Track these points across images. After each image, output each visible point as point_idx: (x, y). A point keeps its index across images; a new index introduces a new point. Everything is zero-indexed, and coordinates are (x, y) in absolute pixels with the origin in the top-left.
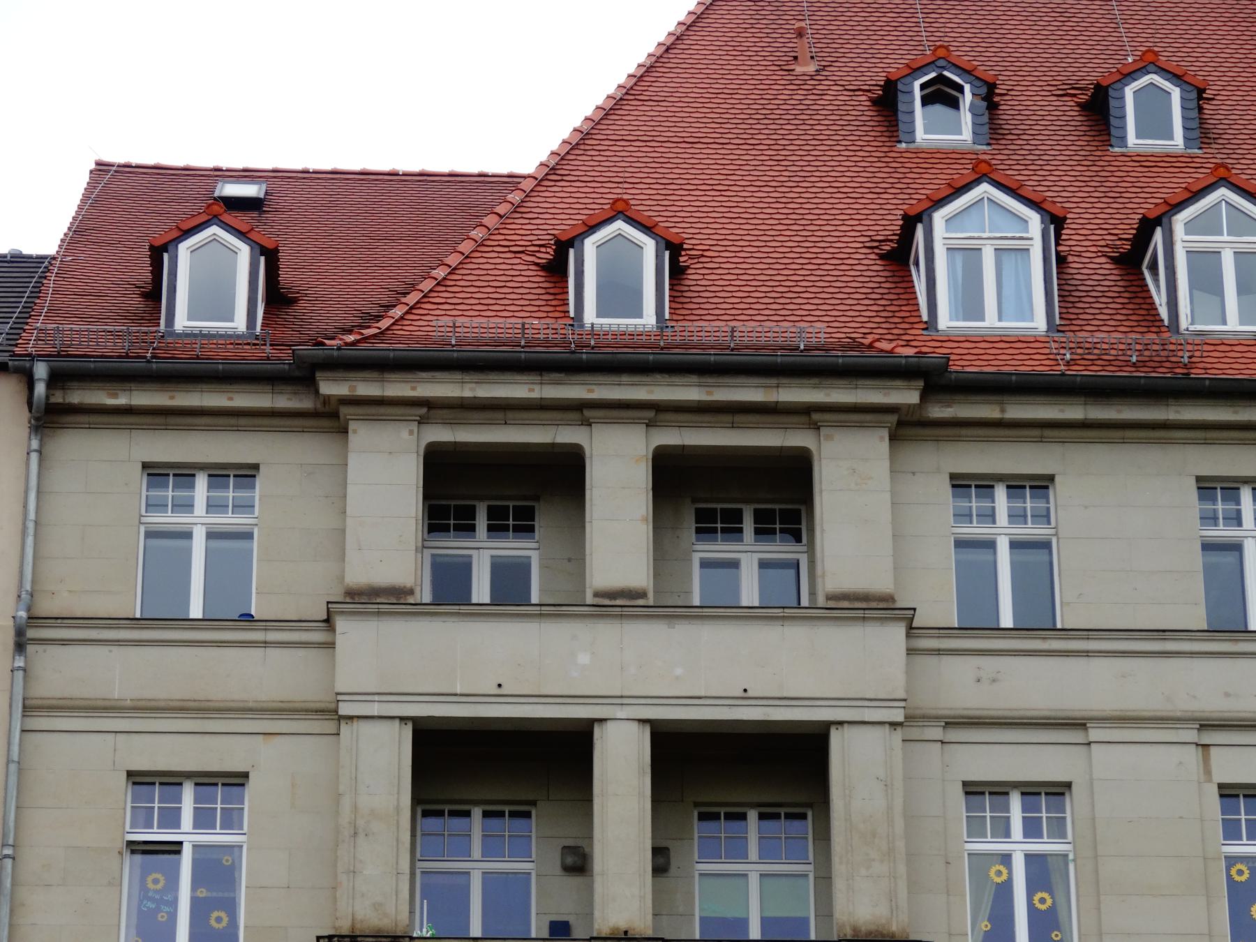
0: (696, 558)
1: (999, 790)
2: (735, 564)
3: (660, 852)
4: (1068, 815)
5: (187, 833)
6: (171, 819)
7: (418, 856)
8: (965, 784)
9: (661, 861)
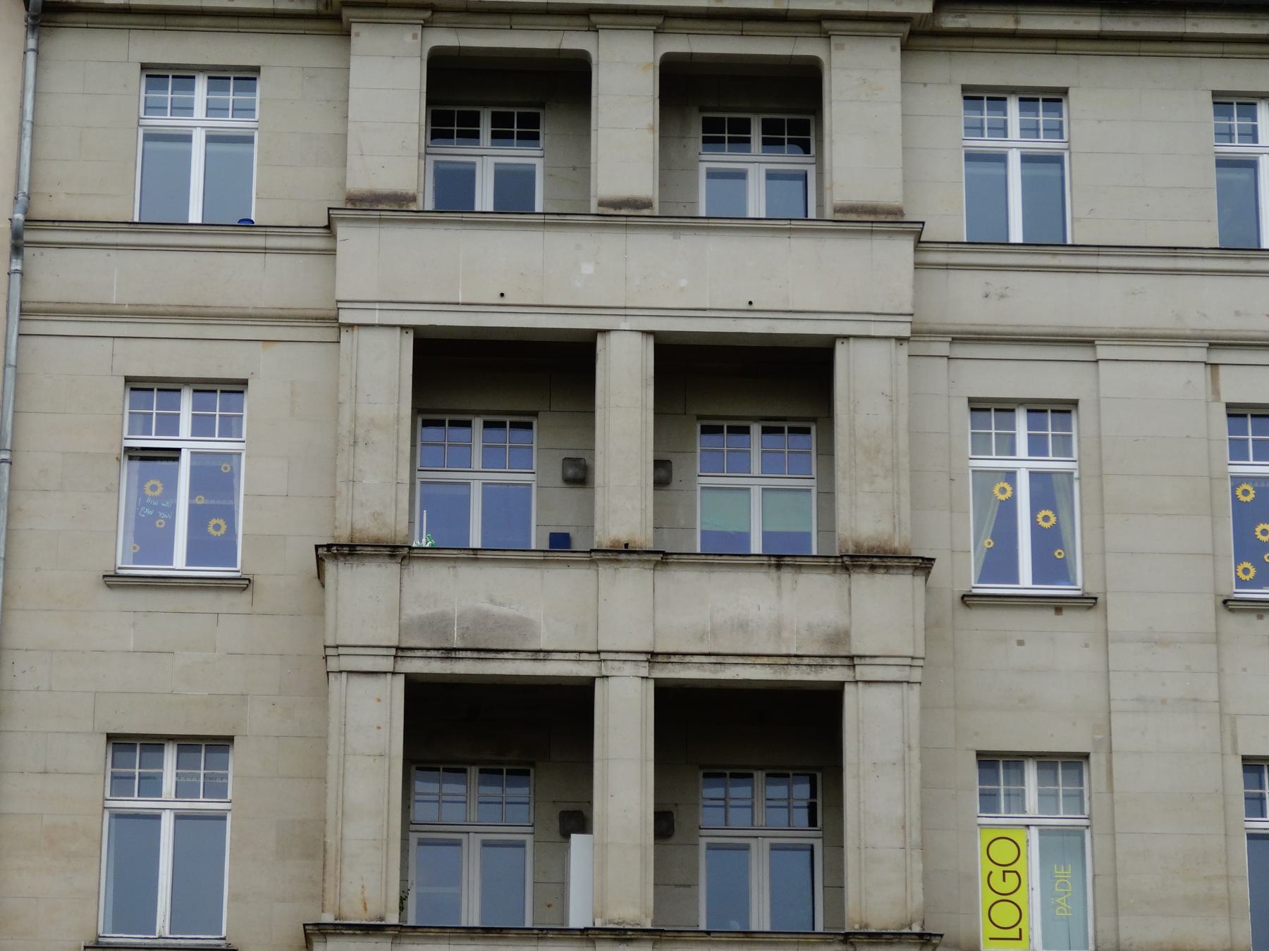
0: (703, 842)
1: (1005, 407)
2: (746, 848)
3: (660, 464)
4: (1074, 433)
5: (185, 439)
6: (151, 786)
7: (418, 466)
8: (971, 400)
9: (663, 473)
